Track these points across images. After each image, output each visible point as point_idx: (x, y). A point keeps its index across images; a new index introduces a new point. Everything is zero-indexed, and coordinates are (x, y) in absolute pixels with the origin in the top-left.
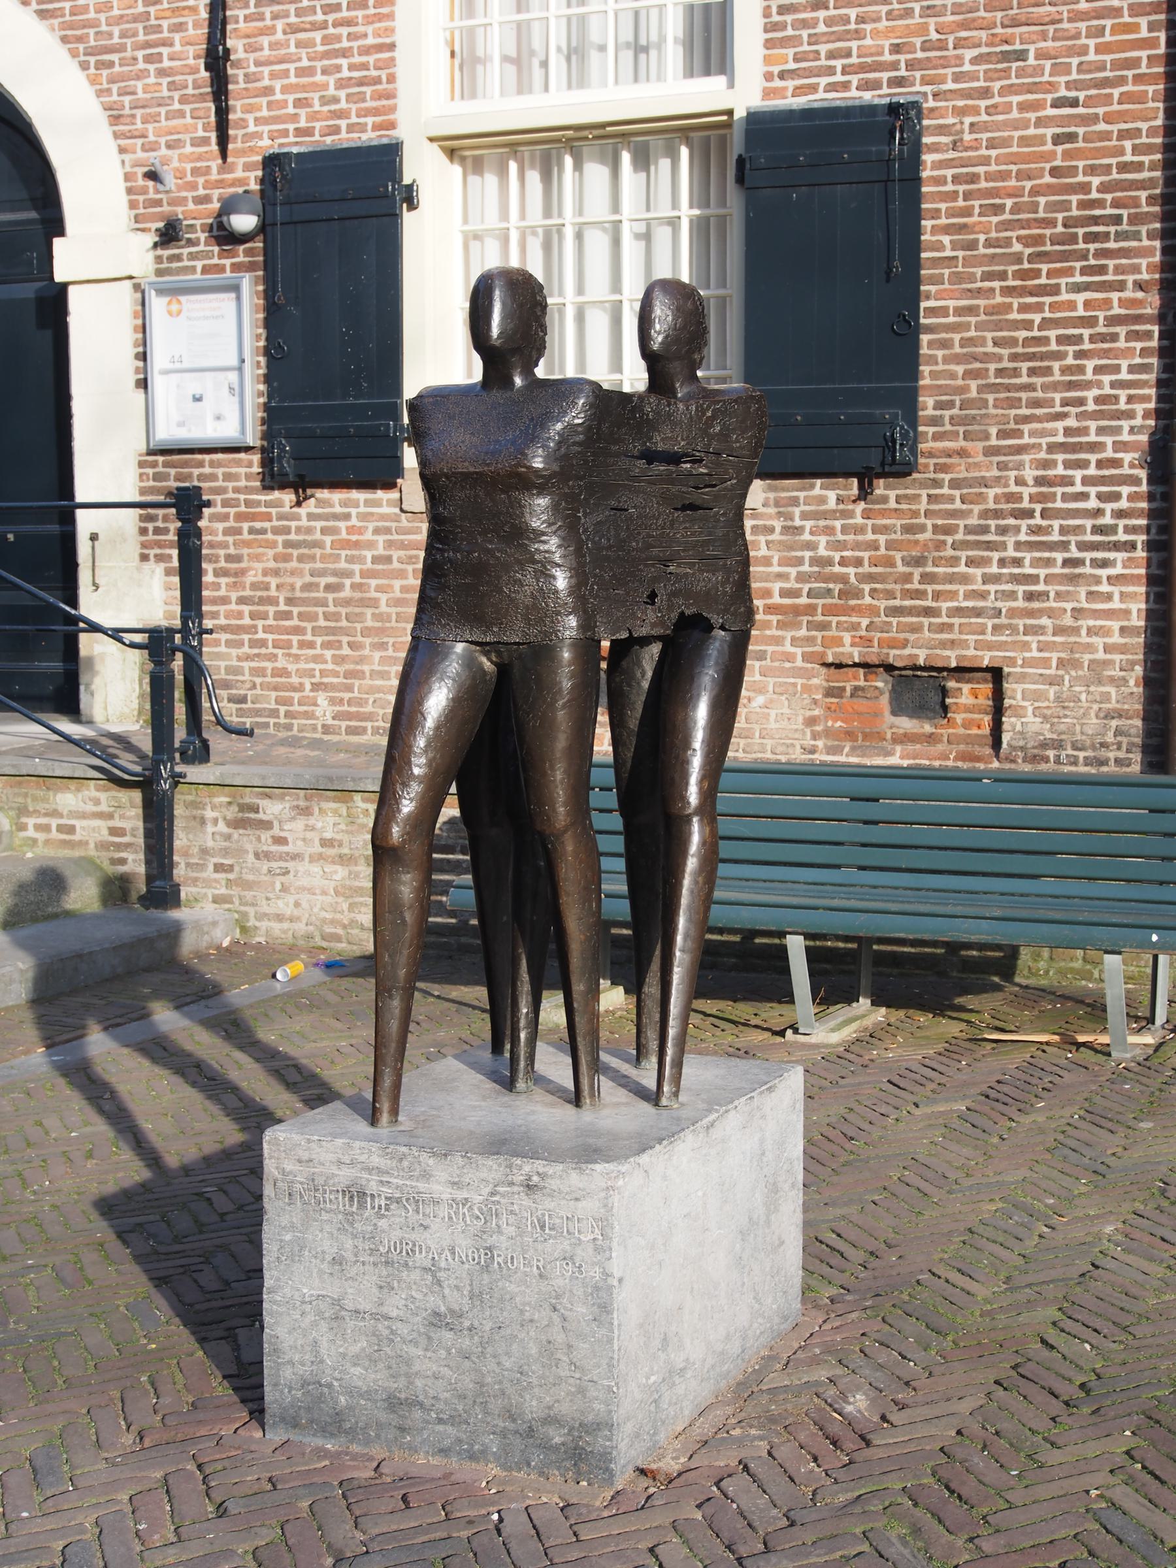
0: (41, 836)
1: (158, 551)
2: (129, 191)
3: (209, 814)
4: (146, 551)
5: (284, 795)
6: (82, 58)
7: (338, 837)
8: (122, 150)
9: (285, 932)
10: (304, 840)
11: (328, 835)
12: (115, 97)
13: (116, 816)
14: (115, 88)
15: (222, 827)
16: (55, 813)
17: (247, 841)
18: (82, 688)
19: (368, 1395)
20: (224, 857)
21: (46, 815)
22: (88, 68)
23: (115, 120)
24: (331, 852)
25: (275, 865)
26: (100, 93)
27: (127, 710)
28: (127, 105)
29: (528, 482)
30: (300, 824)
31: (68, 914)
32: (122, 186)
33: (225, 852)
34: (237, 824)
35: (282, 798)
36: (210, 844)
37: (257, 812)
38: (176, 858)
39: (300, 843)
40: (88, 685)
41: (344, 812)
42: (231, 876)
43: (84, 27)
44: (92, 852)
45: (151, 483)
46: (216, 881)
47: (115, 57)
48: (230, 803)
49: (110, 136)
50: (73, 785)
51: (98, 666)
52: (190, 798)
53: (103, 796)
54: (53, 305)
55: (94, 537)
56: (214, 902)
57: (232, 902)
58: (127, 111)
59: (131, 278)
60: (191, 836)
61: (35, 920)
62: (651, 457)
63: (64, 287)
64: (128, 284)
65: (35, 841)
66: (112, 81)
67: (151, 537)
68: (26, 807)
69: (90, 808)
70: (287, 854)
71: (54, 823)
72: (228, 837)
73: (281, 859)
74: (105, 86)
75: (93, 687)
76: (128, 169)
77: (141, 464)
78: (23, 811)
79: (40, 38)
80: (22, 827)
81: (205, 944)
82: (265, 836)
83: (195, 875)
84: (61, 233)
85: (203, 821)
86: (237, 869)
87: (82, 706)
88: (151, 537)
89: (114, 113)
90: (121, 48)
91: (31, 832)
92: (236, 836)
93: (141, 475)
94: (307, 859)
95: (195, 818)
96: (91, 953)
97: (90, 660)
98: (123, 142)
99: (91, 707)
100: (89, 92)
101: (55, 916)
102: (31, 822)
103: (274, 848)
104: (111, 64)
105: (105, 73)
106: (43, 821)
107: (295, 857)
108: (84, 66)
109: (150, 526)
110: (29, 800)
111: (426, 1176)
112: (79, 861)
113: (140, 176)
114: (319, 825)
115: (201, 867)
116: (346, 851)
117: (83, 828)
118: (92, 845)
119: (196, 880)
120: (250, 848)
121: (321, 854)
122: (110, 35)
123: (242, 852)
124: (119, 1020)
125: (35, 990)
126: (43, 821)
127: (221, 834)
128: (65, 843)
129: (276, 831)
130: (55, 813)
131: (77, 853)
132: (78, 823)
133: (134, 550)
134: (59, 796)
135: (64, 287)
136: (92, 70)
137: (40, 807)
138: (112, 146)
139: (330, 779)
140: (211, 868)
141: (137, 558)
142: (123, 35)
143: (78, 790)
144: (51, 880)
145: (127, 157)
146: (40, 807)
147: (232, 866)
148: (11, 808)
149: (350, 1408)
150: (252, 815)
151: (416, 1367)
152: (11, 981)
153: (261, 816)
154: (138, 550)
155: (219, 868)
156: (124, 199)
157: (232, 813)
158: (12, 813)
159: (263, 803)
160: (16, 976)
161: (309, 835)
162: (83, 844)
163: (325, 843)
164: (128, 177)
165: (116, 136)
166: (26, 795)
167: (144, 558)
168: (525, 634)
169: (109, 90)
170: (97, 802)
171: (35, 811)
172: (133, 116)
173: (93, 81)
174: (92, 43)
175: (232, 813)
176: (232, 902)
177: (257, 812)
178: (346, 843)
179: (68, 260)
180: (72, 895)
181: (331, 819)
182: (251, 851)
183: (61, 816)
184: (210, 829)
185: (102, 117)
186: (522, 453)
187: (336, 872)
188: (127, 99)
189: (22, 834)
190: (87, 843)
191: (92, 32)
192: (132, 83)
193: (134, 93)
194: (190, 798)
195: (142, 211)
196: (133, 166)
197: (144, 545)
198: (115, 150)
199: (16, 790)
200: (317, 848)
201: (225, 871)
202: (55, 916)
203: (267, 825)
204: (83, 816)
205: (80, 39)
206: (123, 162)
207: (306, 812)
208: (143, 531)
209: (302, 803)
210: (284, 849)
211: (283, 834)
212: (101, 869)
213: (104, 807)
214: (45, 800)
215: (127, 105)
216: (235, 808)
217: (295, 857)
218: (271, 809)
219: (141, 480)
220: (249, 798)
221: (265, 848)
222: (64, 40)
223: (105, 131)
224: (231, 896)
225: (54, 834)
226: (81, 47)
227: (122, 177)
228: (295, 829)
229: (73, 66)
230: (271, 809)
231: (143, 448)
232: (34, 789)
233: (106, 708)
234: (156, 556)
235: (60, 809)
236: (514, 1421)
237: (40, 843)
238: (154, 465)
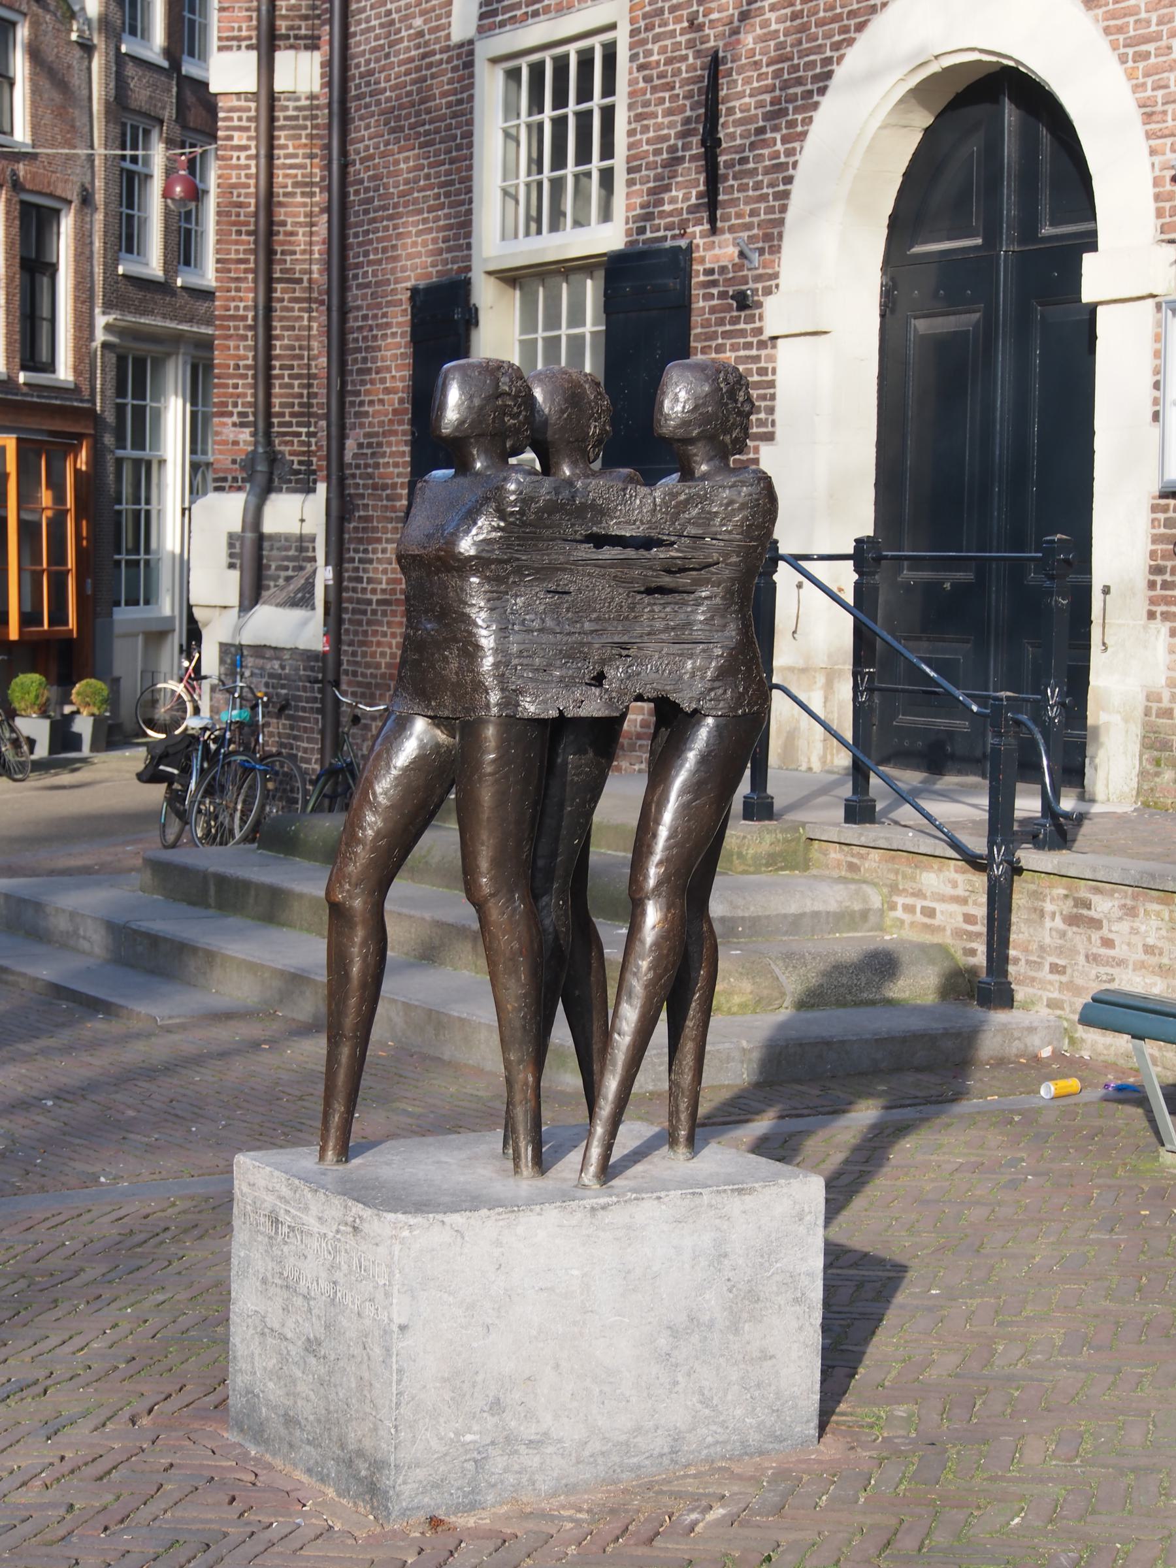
0: (907, 917)
1: (1164, 608)
2: (1157, 197)
3: (1049, 907)
4: (1154, 608)
5: (1114, 891)
6: (1122, 50)
7: (1159, 944)
8: (1153, 152)
9: (1108, 1047)
10: (1129, 944)
11: (1151, 941)
12: (1149, 93)
13: (970, 902)
14: (1149, 81)
15: (1058, 923)
16: (919, 894)
17: (1078, 937)
18: (1087, 761)
19: (275, 1408)
20: (1058, 956)
21: (913, 895)
22: (1126, 62)
23: (1148, 117)
24: (1153, 960)
25: (1102, 970)
26: (1136, 88)
27: (1126, 789)
28: (1160, 101)
29: (463, 566)
30: (1124, 926)
31: (889, 1003)
32: (1150, 191)
33: (1060, 951)
34: (1073, 920)
35: (1111, 894)
36: (1048, 940)
37: (1089, 909)
38: (1012, 953)
39: (1125, 947)
40: (1093, 758)
41: (1166, 916)
42: (1064, 979)
43: (1125, 16)
44: (947, 939)
45: (1162, 530)
46: (1051, 983)
47: (1150, 47)
48: (1066, 896)
49: (1142, 135)
50: (936, 863)
51: (1103, 738)
52: (1033, 887)
53: (960, 878)
54: (1083, 330)
55: (1106, 590)
56: (1048, 1006)
57: (1062, 1009)
58: (1159, 108)
59: (1155, 296)
60: (1031, 930)
61: (841, 1004)
62: (600, 541)
63: (1092, 309)
64: (1151, 302)
65: (902, 922)
66: (1147, 75)
67: (1159, 592)
68: (897, 885)
69: (949, 891)
70: (1114, 958)
71: (919, 904)
72: (1063, 935)
73: (1107, 964)
74: (1141, 80)
75: (1097, 760)
76: (1157, 173)
77: (1154, 509)
78: (894, 889)
79: (1086, 28)
80: (893, 907)
81: (1014, 1051)
82: (1096, 936)
83: (1033, 974)
84: (1090, 242)
85: (1042, 914)
86: (1069, 971)
87: (1086, 782)
88: (1159, 592)
89: (1148, 110)
90: (1157, 37)
91: (899, 913)
92: (1070, 934)
93: (1153, 520)
94: (1131, 967)
95: (1035, 910)
96: (843, 1042)
97: (1096, 728)
98: (1153, 143)
99: (1094, 783)
100: (1125, 87)
101: (873, 1003)
102: (900, 901)
103: (1103, 951)
104: (1147, 55)
105: (1141, 65)
106: (910, 901)
107: (1121, 963)
108: (1123, 59)
109: (1159, 579)
110: (900, 877)
111: (306, 1209)
112: (923, 948)
113: (1168, 179)
114: (1143, 928)
115: (1037, 965)
116: (1165, 961)
117: (942, 912)
118: (948, 932)
119: (1033, 979)
120: (1081, 948)
121: (1143, 962)
122: (1148, 22)
123: (1073, 951)
124: (805, 1112)
125: (761, 1073)
126: (910, 901)
127: (1057, 931)
128: (927, 927)
129: (1105, 932)
130: (919, 894)
131: (936, 939)
132: (939, 907)
133: (1143, 607)
134: (925, 875)
135: (1092, 309)
136: (1130, 64)
137: (909, 885)
138: (1143, 146)
139: (1152, 876)
140: (1047, 968)
141: (1145, 615)
142: (1160, 22)
143: (940, 870)
144: (883, 964)
145: (1157, 159)
146: (909, 885)
147: (1064, 967)
148: (885, 885)
149: (267, 1419)
150: (1085, 912)
151: (299, 1389)
152: (729, 1059)
153: (1092, 913)
154: (1145, 607)
155: (1055, 969)
156: (1151, 206)
157: (1068, 907)
158: (885, 890)
159: (1096, 899)
160: (736, 1054)
161: (1135, 939)
162: (940, 929)
163: (1149, 950)
164: (1157, 182)
165: (1149, 136)
166: (897, 872)
167: (1151, 615)
168: (454, 710)
169: (1144, 85)
170: (955, 885)
171: (904, 890)
172: (1165, 113)
173: (1130, 76)
174: (1132, 33)
175: (1068, 907)
176: (1062, 1009)
177: (1089, 909)
178: (1166, 953)
179: (1097, 278)
180: (901, 983)
181: (1154, 923)
182: (1083, 952)
183: (925, 897)
184: (1048, 924)
185: (1136, 115)
186: (452, 540)
187: (1155, 984)
188: (1160, 93)
189: (892, 914)
190: (944, 929)
191: (1131, 20)
192: (1165, 75)
193: (1166, 87)
194: (1033, 887)
195: (1168, 220)
196: (1162, 170)
197: (1153, 601)
198: (1146, 151)
199: (890, 865)
200: (1140, 955)
201: (1058, 972)
202: (873, 1003)
203: (1096, 924)
204: (943, 899)
205: (1120, 30)
206: (1153, 165)
207: (1131, 912)
208: (1152, 585)
209: (1129, 902)
210: (1111, 952)
211: (1111, 936)
212: (953, 958)
213: (960, 892)
214: (913, 879)
215: (1160, 101)
216: (1070, 902)
217: (1121, 963)
218: (1103, 906)
219: (1153, 527)
220: (1084, 894)
221: (1095, 950)
222: (1107, 31)
223: (1138, 130)
224: (1062, 1001)
225: (919, 917)
226: (1121, 38)
227: (1150, 182)
228: (1119, 930)
229: (1112, 59)
230: (1103, 906)
231: (1155, 489)
232: (903, 865)
233: (1107, 786)
234: (1162, 613)
235: (924, 889)
236: (343, 1450)
237: (907, 925)
238: (1165, 509)
